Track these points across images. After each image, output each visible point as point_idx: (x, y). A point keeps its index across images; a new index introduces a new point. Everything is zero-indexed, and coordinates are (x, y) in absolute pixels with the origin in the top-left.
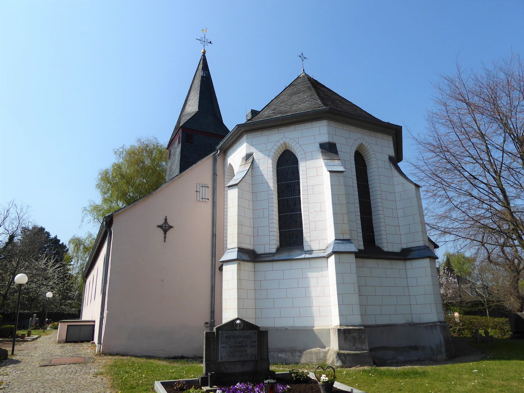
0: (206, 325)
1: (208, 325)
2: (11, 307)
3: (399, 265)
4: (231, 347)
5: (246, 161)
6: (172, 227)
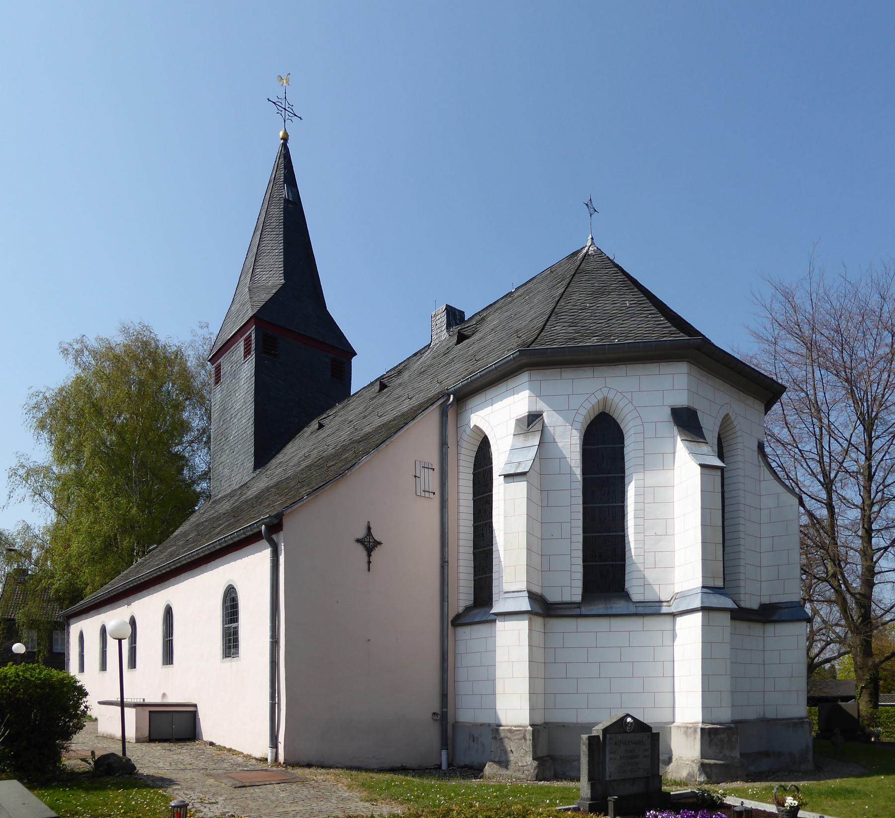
0: (434, 717)
1: (439, 716)
2: (866, 721)
3: (757, 628)
4: (621, 757)
5: (528, 426)
6: (380, 543)
